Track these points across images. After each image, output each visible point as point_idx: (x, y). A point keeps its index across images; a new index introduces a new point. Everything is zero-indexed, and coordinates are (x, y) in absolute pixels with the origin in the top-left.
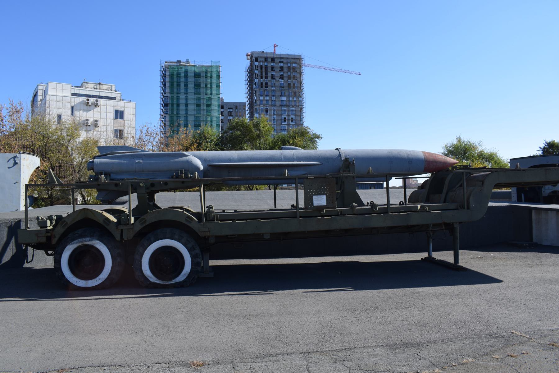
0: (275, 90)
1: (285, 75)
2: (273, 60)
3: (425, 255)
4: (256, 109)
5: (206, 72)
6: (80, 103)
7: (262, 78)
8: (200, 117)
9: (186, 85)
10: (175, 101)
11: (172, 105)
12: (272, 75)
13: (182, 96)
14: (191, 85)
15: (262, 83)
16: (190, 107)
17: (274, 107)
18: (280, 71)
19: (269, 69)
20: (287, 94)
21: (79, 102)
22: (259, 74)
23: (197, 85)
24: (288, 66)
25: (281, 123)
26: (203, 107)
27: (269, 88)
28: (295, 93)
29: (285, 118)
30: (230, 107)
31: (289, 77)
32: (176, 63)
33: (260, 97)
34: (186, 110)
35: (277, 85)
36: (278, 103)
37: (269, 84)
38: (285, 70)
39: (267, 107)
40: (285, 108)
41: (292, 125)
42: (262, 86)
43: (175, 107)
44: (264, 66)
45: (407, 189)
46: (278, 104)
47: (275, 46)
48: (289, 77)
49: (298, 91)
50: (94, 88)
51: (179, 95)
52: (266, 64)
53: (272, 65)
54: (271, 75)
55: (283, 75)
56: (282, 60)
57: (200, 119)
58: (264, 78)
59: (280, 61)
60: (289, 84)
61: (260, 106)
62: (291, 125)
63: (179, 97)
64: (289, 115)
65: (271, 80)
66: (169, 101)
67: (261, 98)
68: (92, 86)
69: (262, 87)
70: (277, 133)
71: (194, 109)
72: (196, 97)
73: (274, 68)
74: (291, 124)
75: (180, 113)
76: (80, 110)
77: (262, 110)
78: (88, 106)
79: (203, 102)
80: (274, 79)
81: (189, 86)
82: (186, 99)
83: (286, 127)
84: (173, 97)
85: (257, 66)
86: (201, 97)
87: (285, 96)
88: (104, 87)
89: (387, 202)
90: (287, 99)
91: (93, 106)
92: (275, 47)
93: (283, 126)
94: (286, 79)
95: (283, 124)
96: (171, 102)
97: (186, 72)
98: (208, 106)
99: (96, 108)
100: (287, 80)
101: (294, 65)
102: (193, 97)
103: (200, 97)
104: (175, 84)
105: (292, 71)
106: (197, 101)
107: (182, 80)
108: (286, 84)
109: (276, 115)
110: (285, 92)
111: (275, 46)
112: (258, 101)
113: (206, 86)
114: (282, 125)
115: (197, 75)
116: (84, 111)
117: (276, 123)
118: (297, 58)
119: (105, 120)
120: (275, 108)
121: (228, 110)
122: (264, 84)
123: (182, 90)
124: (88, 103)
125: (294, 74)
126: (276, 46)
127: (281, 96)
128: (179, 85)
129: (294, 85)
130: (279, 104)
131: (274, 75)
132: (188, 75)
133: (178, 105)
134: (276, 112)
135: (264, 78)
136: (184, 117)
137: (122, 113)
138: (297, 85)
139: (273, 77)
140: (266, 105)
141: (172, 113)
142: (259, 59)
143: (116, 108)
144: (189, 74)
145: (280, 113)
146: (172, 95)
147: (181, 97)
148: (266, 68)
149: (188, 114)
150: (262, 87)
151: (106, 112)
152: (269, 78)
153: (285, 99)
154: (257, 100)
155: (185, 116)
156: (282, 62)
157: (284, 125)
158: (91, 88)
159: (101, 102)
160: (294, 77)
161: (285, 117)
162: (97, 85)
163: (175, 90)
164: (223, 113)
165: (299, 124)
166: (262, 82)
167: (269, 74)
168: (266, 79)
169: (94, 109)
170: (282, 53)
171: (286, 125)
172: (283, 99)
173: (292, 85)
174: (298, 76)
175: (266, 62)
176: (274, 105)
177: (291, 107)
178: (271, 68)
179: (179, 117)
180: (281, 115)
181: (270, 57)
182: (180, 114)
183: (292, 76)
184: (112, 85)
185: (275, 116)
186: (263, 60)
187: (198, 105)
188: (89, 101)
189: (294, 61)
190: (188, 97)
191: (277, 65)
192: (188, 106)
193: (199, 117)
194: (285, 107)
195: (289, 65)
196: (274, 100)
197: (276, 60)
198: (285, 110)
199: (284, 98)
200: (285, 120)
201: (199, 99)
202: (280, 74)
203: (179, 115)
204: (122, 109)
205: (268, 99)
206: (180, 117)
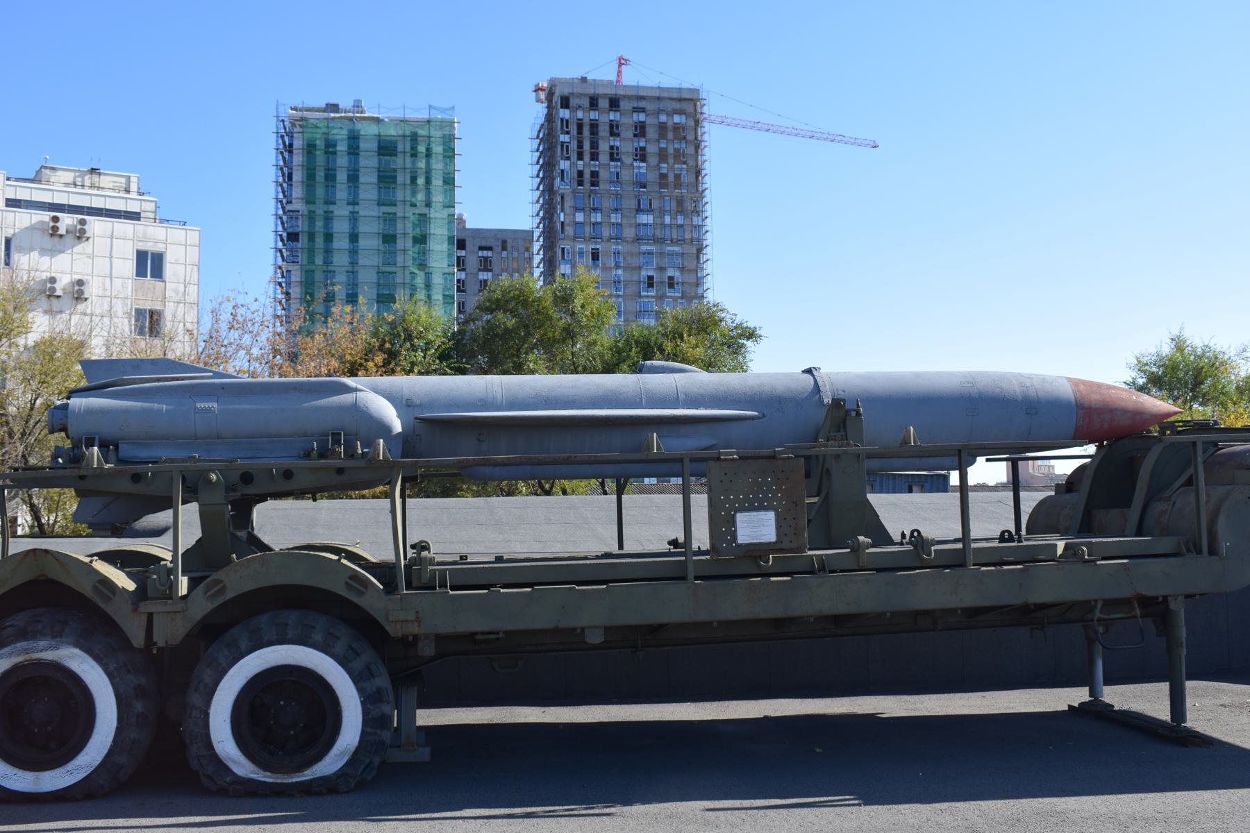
0: (620, 192)
1: (652, 149)
2: (614, 103)
3: (1079, 695)
4: (563, 249)
5: (414, 138)
6: (32, 228)
7: (580, 157)
8: (395, 273)
9: (353, 178)
10: (319, 224)
11: (312, 237)
12: (612, 148)
13: (341, 211)
14: (368, 178)
15: (580, 174)
16: (363, 243)
17: (618, 244)
18: (635, 135)
19: (604, 131)
20: (655, 204)
21: (27, 224)
22: (574, 145)
23: (386, 179)
24: (661, 123)
27: (603, 186)
28: (680, 202)
29: (650, 278)
30: (484, 244)
31: (662, 155)
32: (324, 110)
33: (574, 215)
34: (354, 252)
35: (627, 178)
36: (629, 233)
37: (603, 175)
38: (652, 133)
39: (596, 243)
40: (649, 248)
41: (671, 297)
42: (582, 181)
43: (319, 241)
44: (586, 121)
46: (629, 236)
47: (622, 62)
48: (662, 155)
49: (689, 195)
50: (75, 185)
51: (331, 207)
52: (594, 115)
53: (612, 118)
54: (607, 149)
55: (643, 149)
56: (642, 104)
57: (393, 279)
58: (587, 157)
59: (634, 108)
60: (663, 176)
62: (667, 297)
63: (332, 212)
64: (661, 269)
65: (609, 165)
67: (580, 217)
68: (69, 177)
69: (580, 183)
70: (625, 321)
71: (377, 248)
72: (384, 213)
73: (617, 128)
74: (667, 294)
76: (32, 249)
77: (581, 253)
78: (56, 239)
79: (406, 228)
80: (619, 160)
81: (362, 180)
82: (354, 218)
84: (314, 212)
85: (567, 121)
87: (650, 210)
88: (105, 181)
90: (658, 221)
91: (69, 239)
92: (620, 65)
93: (646, 300)
94: (653, 160)
95: (643, 294)
96: (571, 243)
97: (354, 138)
98: (421, 240)
99: (80, 243)
100: (658, 165)
101: (677, 119)
102: (376, 214)
103: (395, 214)
104: (320, 175)
105: (670, 135)
106: (385, 225)
107: (342, 161)
108: (652, 177)
109: (624, 268)
110: (650, 200)
111: (622, 62)
112: (568, 225)
113: (414, 180)
114: (640, 297)
115: (386, 148)
116: (44, 251)
118: (688, 97)
119: (108, 280)
120: (620, 247)
121: (480, 253)
122: (587, 176)
123: (342, 193)
124: (55, 229)
125: (677, 146)
126: (623, 62)
127: (639, 210)
128: (330, 177)
129: (678, 177)
130: (633, 236)
131: (617, 148)
132: (358, 147)
133: (329, 237)
134: (624, 259)
135: (587, 157)
136: (347, 272)
137: (158, 259)
138: (687, 178)
139: (614, 155)
140: (594, 238)
141: (311, 261)
142: (573, 102)
143: (140, 244)
144: (363, 145)
145: (635, 262)
147: (336, 213)
148: (594, 126)
149: (357, 263)
150: (580, 183)
151: (111, 257)
152: (604, 158)
153: (651, 222)
154: (566, 222)
155: (446, 271)
156: (643, 110)
157: (647, 297)
158: (67, 185)
159: (96, 226)
160: (679, 155)
161: (651, 273)
162: (83, 174)
163: (320, 192)
164: (463, 260)
165: (693, 294)
166: (581, 168)
167: (604, 147)
168: (592, 159)
169: (72, 248)
170: (640, 84)
171: (652, 297)
172: (645, 222)
173: (671, 178)
174: (691, 150)
175: (594, 110)
176: (618, 238)
177: (667, 245)
178: (608, 128)
179: (330, 272)
180: (640, 268)
181: (604, 96)
182: (335, 264)
183: (671, 151)
184: (129, 176)
185: (620, 272)
186: (586, 103)
187: (389, 239)
188: (58, 224)
189: (677, 106)
190: (358, 213)
191: (628, 121)
192: (357, 242)
193: (390, 273)
194: (650, 245)
195: (663, 118)
196: (617, 224)
197: (624, 105)
198: (650, 253)
199: (647, 219)
200: (650, 282)
201: (391, 219)
202: (636, 145)
204: (159, 248)
205: (599, 220)
206: (334, 272)
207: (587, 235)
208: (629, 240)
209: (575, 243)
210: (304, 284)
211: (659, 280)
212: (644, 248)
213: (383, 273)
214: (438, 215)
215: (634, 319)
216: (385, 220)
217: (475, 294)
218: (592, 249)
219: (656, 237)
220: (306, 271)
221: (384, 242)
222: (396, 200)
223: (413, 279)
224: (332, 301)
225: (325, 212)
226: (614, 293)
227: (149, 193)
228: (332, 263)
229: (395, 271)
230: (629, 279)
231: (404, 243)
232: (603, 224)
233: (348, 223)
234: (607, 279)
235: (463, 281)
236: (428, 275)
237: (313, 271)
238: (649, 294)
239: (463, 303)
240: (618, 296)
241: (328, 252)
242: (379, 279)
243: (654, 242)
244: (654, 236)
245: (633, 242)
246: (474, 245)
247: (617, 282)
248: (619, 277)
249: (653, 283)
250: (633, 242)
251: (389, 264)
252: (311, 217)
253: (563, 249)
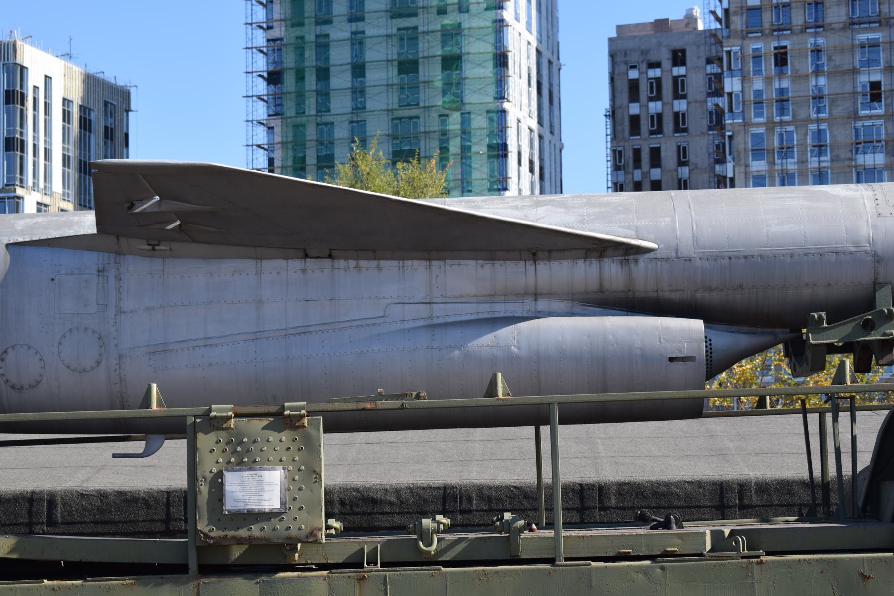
8: (418, 117)
10: (310, 54)
11: (300, 77)
13: (339, 32)
16: (373, 76)
17: (816, 35)
25: (856, 112)
26: (432, 73)
29: (875, 86)
34: (358, 92)
39: (779, 38)
40: (871, 36)
43: (311, 82)
45: (808, 415)
46: (836, 19)
57: (416, 126)
61: (743, 38)
63: (327, 36)
66: (289, 60)
70: (832, 161)
71: (385, 83)
72: (399, 29)
74: (753, 121)
75: (332, 106)
82: (357, 41)
83: (878, 129)
86: (421, 29)
89: (853, 472)
93: (868, 123)
96: (739, 42)
98: (452, 62)
102: (383, 32)
103: (416, 28)
106: (402, 46)
109: (830, 75)
112: (735, 13)
114: (857, 117)
117: (830, 113)
120: (820, 41)
133: (323, 74)
134: (830, 59)
140: (779, 29)
141: (300, 112)
145: (844, 61)
146: (297, 32)
147: (368, 33)
149: (364, 108)
154: (732, 10)
155: (492, 107)
157: (870, 117)
161: (875, 78)
164: (683, 82)
171: (878, 117)
179: (326, 124)
180: (854, 71)
182: (332, 112)
185: (822, 81)
190: (363, 32)
192: (363, 76)
193: (411, 118)
194: (873, 30)
198: (874, 45)
201: (410, 37)
203: (327, 119)
206: (332, 123)
207: (767, 25)
208: (836, 26)
209: (746, 42)
210: (290, 146)
211: (889, 88)
212: (862, 37)
213: (400, 119)
214: (475, 23)
215: (849, 155)
216: (402, 39)
217: (703, 133)
218: (776, 48)
219: (883, 16)
220: (294, 126)
221: (401, 72)
222: (417, 8)
223: (443, 123)
224: (328, 167)
225: (317, 36)
226: (814, 116)
227: (31, 36)
228: (329, 111)
229: (446, 113)
230: (839, 91)
231: (891, 55)
232: (793, 5)
233: (349, 51)
234: (802, 94)
235: (684, 115)
236: (466, 118)
237: (304, 125)
238: (874, 112)
239: (685, 148)
240: (818, 121)
241: (324, 95)
242: (395, 127)
243: (880, 25)
244: (879, 15)
245: (844, 29)
246: (699, 57)
247: (819, 98)
248: (820, 90)
249: (880, 95)
250: (844, 29)
251: (409, 105)
252: (300, 46)
253: (729, 53)
